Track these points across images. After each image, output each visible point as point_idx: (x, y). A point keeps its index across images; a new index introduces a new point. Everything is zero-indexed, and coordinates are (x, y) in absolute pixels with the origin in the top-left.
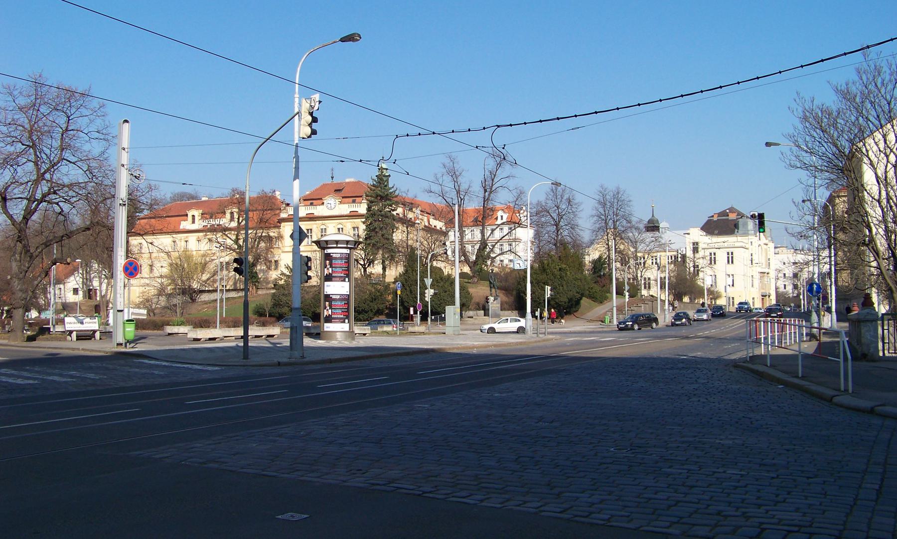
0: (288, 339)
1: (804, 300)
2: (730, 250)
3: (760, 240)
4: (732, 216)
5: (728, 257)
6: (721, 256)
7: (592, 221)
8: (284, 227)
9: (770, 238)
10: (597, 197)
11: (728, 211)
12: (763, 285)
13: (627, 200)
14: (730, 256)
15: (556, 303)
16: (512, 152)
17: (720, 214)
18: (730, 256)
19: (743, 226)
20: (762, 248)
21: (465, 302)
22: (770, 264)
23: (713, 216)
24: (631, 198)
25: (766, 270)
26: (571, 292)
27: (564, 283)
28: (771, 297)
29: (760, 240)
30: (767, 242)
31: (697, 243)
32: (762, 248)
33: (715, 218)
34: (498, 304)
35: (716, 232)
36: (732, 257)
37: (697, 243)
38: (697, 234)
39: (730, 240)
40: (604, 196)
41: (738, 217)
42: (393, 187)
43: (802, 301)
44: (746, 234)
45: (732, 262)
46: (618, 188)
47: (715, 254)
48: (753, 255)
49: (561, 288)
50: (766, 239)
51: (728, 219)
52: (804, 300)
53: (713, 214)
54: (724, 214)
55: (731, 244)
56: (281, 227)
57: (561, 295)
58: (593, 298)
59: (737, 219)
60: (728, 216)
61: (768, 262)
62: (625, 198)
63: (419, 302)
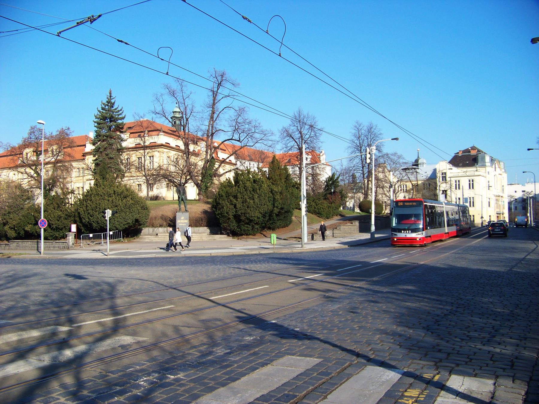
0: (448, 230)
1: (530, 217)
2: (471, 178)
3: (495, 170)
4: (473, 153)
5: (470, 184)
6: (464, 183)
7: (350, 151)
8: (88, 159)
9: (503, 170)
10: (354, 131)
11: (470, 148)
12: (498, 206)
13: (379, 133)
14: (471, 182)
15: (248, 219)
16: (230, 75)
17: (464, 152)
18: (471, 182)
19: (482, 160)
20: (497, 178)
21: (139, 218)
22: (504, 190)
23: (458, 153)
24: (382, 132)
25: (501, 194)
26: (266, 206)
27: (256, 196)
28: (504, 215)
29: (495, 170)
30: (501, 172)
31: (445, 173)
32: (497, 178)
33: (460, 155)
34: (186, 219)
35: (461, 164)
36: (473, 184)
37: (445, 173)
38: (443, 166)
39: (470, 170)
40: (359, 130)
41: (477, 153)
42: (121, 110)
43: (529, 218)
44: (484, 166)
45: (473, 188)
46: (371, 124)
47: (459, 181)
48: (490, 182)
49: (252, 201)
50: (501, 171)
51: (470, 155)
52: (530, 217)
53: (459, 152)
54: (467, 151)
55: (472, 173)
56: (86, 160)
57: (252, 209)
58: (318, 214)
59: (477, 154)
60: (470, 152)
61: (502, 188)
62: (377, 132)
63: (42, 218)
